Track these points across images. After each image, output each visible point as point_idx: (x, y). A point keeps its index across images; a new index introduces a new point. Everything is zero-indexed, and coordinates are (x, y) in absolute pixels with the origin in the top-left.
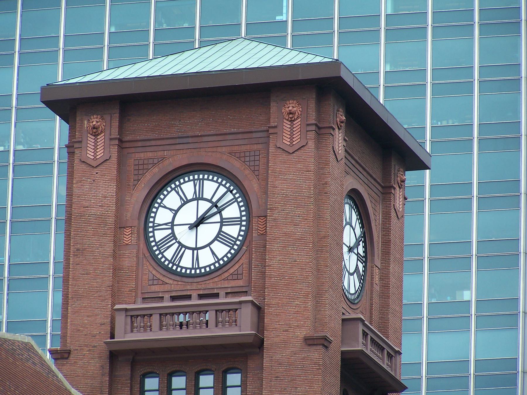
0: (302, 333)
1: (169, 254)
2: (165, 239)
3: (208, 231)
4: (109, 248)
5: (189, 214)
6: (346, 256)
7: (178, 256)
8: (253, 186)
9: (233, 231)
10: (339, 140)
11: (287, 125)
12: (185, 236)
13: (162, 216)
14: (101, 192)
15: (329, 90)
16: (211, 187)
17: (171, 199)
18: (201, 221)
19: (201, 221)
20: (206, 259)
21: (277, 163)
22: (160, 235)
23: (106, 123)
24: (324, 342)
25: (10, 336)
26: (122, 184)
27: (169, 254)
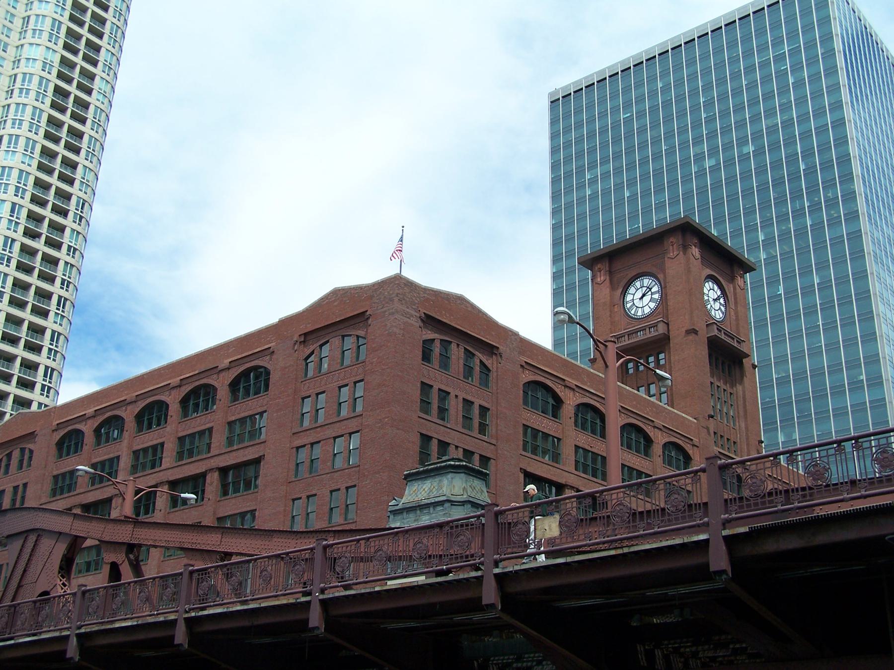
0: (684, 330)
1: (633, 312)
2: (631, 306)
3: (647, 299)
4: (608, 314)
5: (639, 294)
6: (62, 400)
7: (636, 311)
8: (661, 276)
9: (656, 296)
10: (695, 251)
11: (671, 248)
12: (637, 302)
13: (629, 298)
14: (605, 291)
15: (686, 230)
16: (646, 281)
17: (632, 290)
18: (644, 295)
19: (644, 295)
20: (647, 310)
21: (668, 264)
22: (629, 305)
23: (604, 266)
24: (695, 332)
25: (569, 359)
26: (613, 287)
27: (633, 312)
